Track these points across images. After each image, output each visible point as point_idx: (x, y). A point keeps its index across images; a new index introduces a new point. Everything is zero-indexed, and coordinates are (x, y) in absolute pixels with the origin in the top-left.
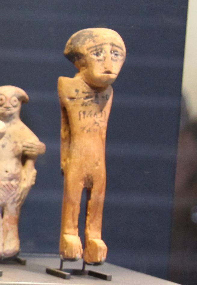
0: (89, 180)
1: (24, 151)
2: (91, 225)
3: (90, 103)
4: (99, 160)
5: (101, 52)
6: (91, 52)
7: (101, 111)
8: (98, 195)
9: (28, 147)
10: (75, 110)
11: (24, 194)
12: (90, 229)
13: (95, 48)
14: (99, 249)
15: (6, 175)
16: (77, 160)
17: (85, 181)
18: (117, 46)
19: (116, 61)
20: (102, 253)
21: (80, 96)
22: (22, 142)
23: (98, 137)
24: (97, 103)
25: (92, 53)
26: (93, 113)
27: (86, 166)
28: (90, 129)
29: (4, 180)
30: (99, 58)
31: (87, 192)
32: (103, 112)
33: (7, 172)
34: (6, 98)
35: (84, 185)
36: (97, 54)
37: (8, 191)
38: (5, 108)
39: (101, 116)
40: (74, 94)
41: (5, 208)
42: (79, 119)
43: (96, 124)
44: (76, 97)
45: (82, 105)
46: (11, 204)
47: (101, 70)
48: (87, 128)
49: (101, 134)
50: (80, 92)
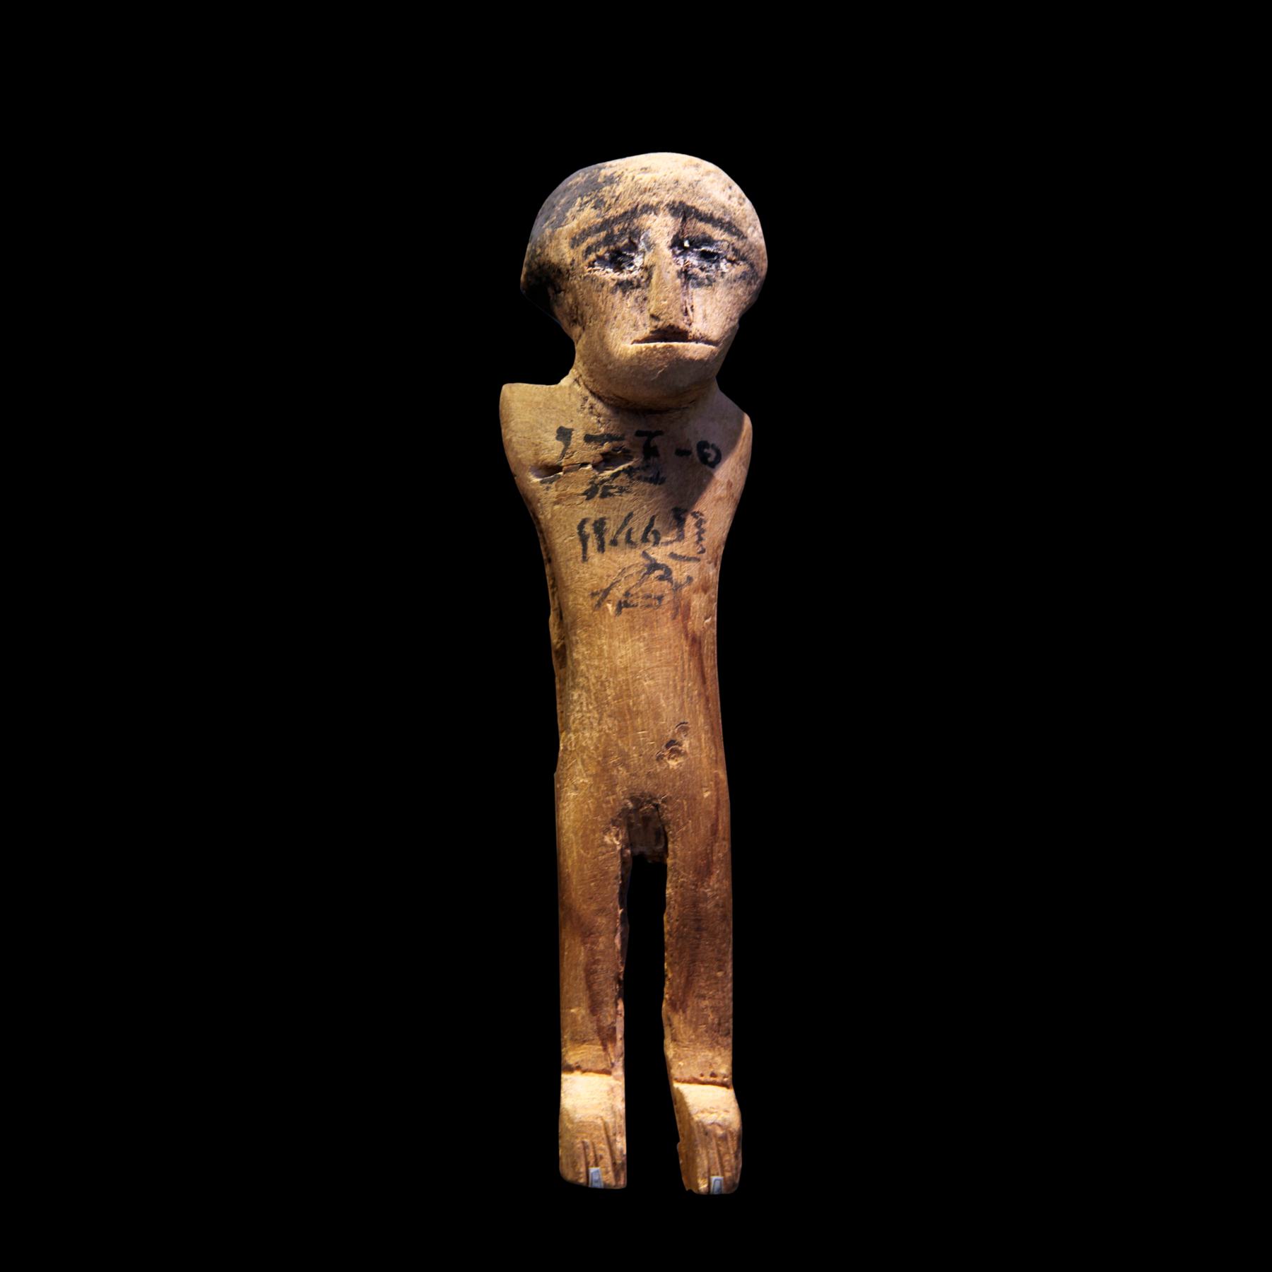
0: (646, 820)
3: (623, 480)
4: (683, 727)
5: (633, 247)
6: (589, 250)
7: (678, 517)
8: (700, 878)
10: (561, 511)
12: (674, 1040)
13: (603, 234)
14: (698, 1136)
16: (589, 738)
18: (709, 219)
19: (711, 282)
20: (714, 1154)
21: (576, 458)
23: (667, 629)
24: (656, 480)
25: (592, 257)
28: (627, 594)
30: (624, 276)
31: (643, 882)
32: (690, 521)
35: (629, 843)
36: (617, 260)
39: (681, 537)
40: (552, 450)
42: (580, 559)
43: (658, 573)
44: (564, 462)
45: (590, 494)
47: (635, 326)
48: (618, 593)
49: (682, 611)
50: (577, 438)
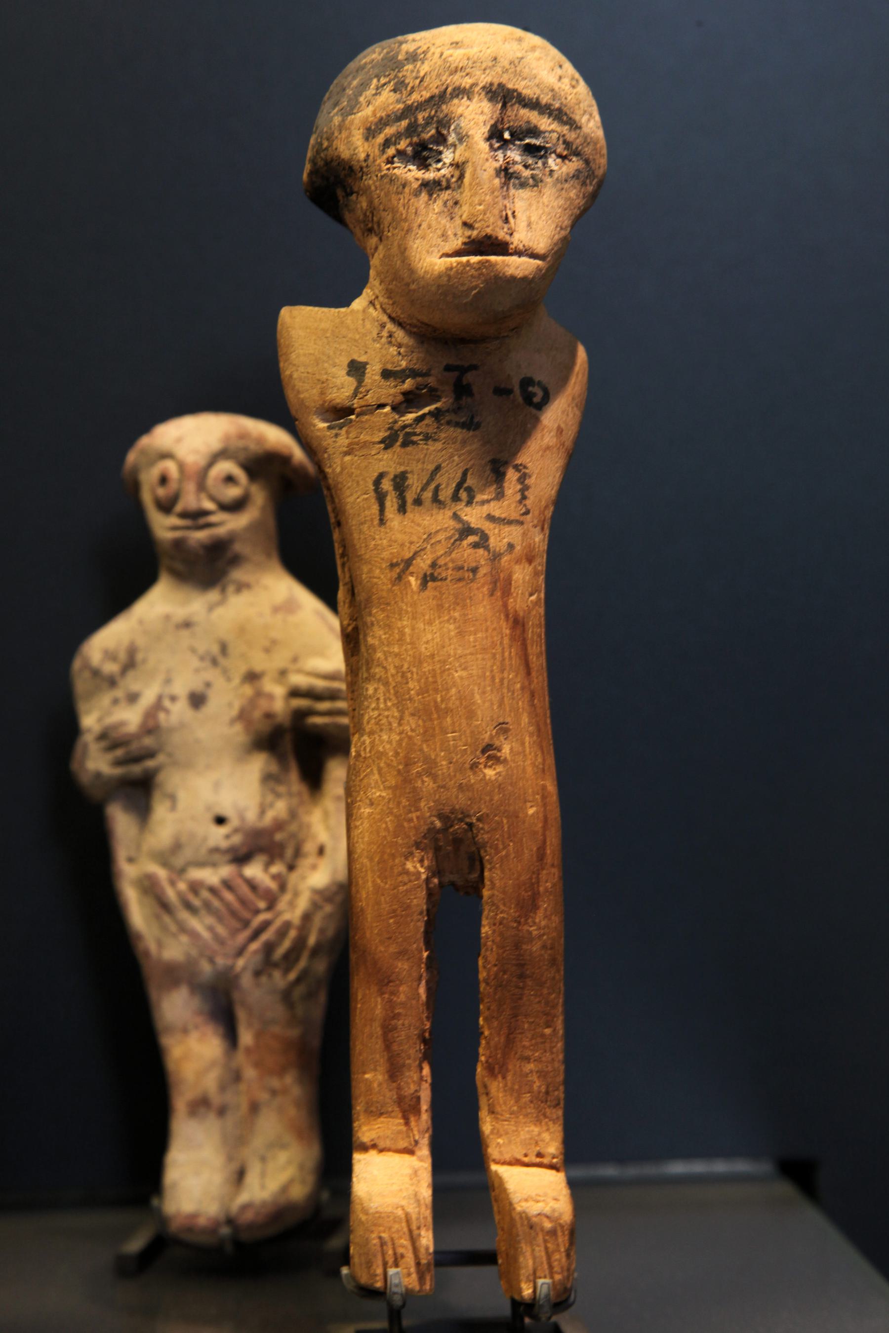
0: (457, 842)
1: (300, 715)
2: (496, 1087)
4: (503, 729)
5: (441, 139)
7: (496, 472)
9: (311, 694)
11: (317, 921)
14: (521, 1229)
15: (218, 836)
17: (437, 849)
18: (534, 105)
19: (536, 182)
21: (371, 399)
22: (283, 673)
23: (483, 607)
24: (470, 425)
25: (391, 151)
26: (447, 482)
27: (430, 770)
28: (434, 565)
29: (214, 865)
30: (430, 175)
32: (512, 475)
33: (220, 821)
34: (181, 466)
35: (436, 871)
36: (422, 155)
37: (233, 913)
38: (184, 515)
39: (500, 495)
40: (342, 388)
41: (236, 996)
43: (472, 539)
44: (356, 403)
45: (388, 443)
46: (257, 974)
48: (423, 564)
49: (501, 586)
